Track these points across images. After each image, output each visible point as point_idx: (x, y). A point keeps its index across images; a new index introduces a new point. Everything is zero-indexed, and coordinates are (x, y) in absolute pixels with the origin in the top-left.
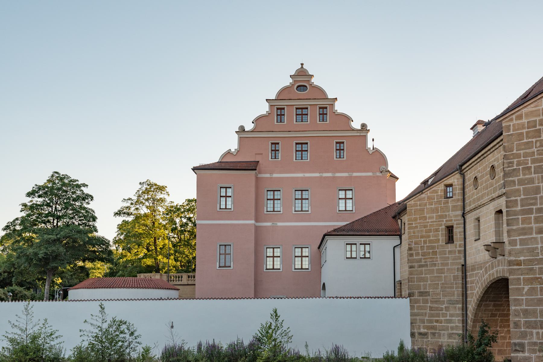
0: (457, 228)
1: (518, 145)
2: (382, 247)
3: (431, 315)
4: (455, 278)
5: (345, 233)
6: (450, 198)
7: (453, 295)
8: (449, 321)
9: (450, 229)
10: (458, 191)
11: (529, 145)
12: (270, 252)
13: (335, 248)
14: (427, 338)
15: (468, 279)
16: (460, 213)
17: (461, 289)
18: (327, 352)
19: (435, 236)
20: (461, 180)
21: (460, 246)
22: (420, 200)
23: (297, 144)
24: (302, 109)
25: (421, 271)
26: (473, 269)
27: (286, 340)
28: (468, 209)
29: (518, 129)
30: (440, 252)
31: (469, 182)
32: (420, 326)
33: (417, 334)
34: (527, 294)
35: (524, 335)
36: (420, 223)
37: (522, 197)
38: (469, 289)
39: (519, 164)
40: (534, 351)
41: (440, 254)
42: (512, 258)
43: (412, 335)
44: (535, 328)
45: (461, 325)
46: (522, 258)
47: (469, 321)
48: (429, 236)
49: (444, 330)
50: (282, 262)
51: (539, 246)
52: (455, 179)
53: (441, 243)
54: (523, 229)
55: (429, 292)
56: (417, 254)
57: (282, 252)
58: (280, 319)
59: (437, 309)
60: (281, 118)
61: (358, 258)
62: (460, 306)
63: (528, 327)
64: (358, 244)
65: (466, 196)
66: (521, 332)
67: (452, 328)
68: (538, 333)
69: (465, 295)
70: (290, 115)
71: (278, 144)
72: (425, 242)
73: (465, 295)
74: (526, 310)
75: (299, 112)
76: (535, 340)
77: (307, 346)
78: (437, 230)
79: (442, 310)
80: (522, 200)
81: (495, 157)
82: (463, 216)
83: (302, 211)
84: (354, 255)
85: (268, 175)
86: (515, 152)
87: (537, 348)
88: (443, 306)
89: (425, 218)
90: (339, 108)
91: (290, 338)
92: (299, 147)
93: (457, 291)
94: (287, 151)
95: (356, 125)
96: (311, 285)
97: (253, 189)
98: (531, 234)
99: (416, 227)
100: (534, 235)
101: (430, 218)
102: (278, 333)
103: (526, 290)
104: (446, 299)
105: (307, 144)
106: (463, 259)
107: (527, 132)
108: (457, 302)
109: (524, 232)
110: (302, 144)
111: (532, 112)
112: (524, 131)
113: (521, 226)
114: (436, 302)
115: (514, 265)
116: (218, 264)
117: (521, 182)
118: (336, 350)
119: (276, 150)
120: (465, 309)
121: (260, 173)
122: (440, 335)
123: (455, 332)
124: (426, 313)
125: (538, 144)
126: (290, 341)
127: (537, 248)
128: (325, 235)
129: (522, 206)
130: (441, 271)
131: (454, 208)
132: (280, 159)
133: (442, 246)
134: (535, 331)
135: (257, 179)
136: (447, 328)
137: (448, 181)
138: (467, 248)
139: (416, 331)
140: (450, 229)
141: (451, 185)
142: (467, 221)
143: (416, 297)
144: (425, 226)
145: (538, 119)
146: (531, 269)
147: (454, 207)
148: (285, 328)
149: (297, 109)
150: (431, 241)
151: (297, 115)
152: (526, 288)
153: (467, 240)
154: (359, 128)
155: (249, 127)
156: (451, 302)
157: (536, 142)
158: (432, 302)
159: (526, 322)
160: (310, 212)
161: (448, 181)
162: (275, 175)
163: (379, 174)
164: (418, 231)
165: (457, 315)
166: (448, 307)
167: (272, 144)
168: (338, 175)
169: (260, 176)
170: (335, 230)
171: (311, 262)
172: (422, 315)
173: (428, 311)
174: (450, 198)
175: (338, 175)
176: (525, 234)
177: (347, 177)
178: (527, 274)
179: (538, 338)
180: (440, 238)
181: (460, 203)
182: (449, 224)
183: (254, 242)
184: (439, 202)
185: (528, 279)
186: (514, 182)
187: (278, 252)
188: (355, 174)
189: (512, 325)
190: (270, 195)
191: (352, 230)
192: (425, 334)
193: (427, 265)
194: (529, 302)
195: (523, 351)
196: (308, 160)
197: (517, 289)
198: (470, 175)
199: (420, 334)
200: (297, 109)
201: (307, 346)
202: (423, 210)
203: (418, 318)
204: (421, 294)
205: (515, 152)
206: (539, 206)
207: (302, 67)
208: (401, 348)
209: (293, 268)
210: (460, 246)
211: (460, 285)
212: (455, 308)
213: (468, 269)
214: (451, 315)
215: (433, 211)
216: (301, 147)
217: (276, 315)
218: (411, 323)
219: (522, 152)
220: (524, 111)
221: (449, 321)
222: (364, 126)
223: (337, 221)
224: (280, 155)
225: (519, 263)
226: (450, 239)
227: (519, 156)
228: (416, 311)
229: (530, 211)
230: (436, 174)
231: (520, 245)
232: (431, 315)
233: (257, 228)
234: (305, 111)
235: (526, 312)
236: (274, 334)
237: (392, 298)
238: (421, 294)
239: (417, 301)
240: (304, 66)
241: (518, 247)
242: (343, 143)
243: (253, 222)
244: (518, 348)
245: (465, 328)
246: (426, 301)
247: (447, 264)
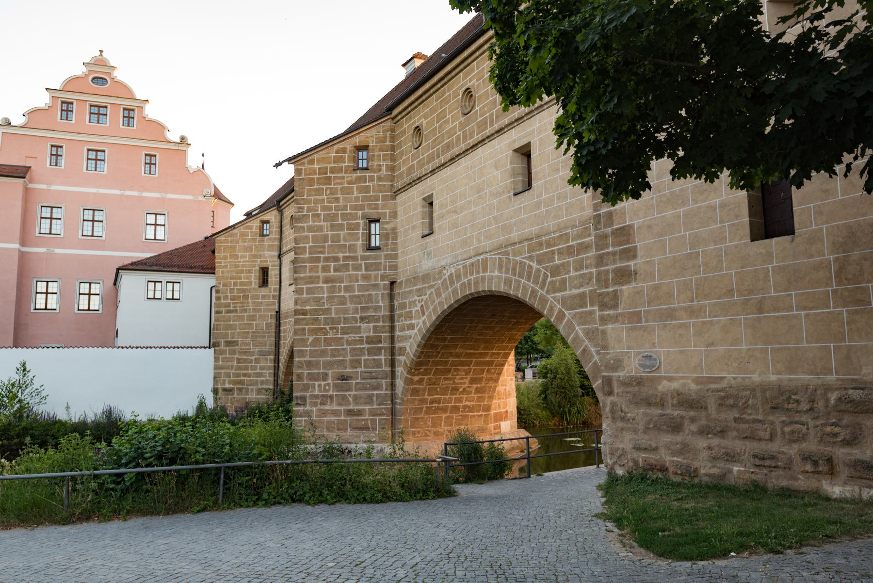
0: (272, 270)
1: (309, 191)
2: (196, 288)
3: (239, 368)
4: (268, 326)
5: (146, 267)
6: (266, 235)
7: (265, 345)
8: (259, 375)
9: (264, 271)
10: (275, 229)
11: (319, 191)
12: (41, 287)
13: (133, 285)
14: (233, 394)
15: (282, 328)
16: (276, 253)
17: (273, 339)
18: (96, 415)
19: (247, 278)
20: (279, 217)
21: (275, 291)
22: (231, 236)
23: (89, 150)
24: (99, 107)
25: (230, 317)
26: (286, 317)
27: (37, 401)
28: (284, 249)
29: (310, 174)
30: (252, 296)
31: (286, 221)
32: (224, 381)
33: (220, 391)
34: (311, 345)
35: (306, 388)
36: (230, 262)
37: (311, 244)
38: (282, 338)
39: (309, 210)
40: (315, 404)
41: (252, 299)
42: (299, 307)
43: (215, 391)
44: (318, 380)
45: (272, 379)
46: (308, 308)
47: (280, 374)
48: (240, 278)
49: (252, 385)
50: (61, 301)
51: (325, 296)
52: (272, 216)
53: (253, 286)
54: (310, 277)
55: (237, 342)
56: (226, 298)
57: (61, 288)
58: (30, 375)
59: (246, 361)
60: (67, 115)
61: (164, 298)
62: (272, 357)
63: (310, 380)
64: (164, 283)
65: (283, 236)
66: (304, 385)
67: (262, 383)
68: (320, 386)
69: (277, 345)
70: (80, 115)
71: (61, 147)
72: (235, 284)
73: (277, 345)
74: (310, 361)
75: (95, 110)
76: (317, 393)
77: (68, 408)
78: (250, 271)
79: (251, 362)
80: (310, 247)
81: (399, 185)
82: (280, 256)
83: (92, 236)
84: (158, 296)
85: (44, 187)
86: (305, 197)
87: (319, 401)
88: (253, 358)
89: (237, 256)
90: (150, 112)
91: (45, 398)
92: (92, 155)
93: (270, 340)
94: (74, 158)
95: (173, 136)
96: (100, 331)
97: (19, 204)
98: (318, 283)
99: (226, 266)
100: (321, 285)
101: (242, 257)
102: (26, 392)
103: (310, 341)
104: (257, 350)
105: (104, 151)
106: (277, 305)
107: (318, 178)
108: (269, 353)
109: (312, 280)
110: (97, 151)
111: (323, 158)
112: (316, 177)
113: (308, 274)
114: (245, 353)
115: (300, 314)
116: (76, 306)
117: (311, 229)
118: (109, 413)
119: (57, 155)
120: (277, 360)
121: (31, 182)
122: (247, 390)
123: (265, 386)
124: (232, 366)
125: (328, 192)
126: (43, 402)
127: (323, 298)
128: (118, 270)
129: (310, 254)
130: (252, 318)
131: (270, 248)
132: (63, 167)
133: (254, 289)
134: (317, 383)
135: (26, 190)
136: (256, 383)
137: (265, 217)
138: (282, 292)
139: (219, 386)
140: (264, 271)
141: (267, 222)
142: (283, 263)
143: (222, 347)
144: (236, 266)
145: (329, 166)
146: (317, 319)
147: (270, 246)
148: (35, 386)
149: (91, 106)
150: (242, 284)
151: (91, 113)
152: (311, 338)
153: (283, 284)
154: (179, 141)
155: (18, 120)
156: (262, 353)
157: (327, 189)
158: (240, 353)
159: (309, 374)
160: (104, 238)
161: (265, 217)
162: (54, 187)
163: (201, 198)
164: (228, 271)
165: (269, 368)
166: (259, 359)
167: (52, 146)
168: (145, 194)
169: (30, 186)
170: (132, 264)
171: (103, 302)
172: (228, 367)
173: (235, 364)
174: (266, 235)
175: (145, 194)
176: (312, 283)
177: (158, 198)
178: (313, 324)
179: (320, 391)
180: (253, 280)
181: (277, 243)
182: (264, 265)
183: (16, 272)
184: (254, 240)
185: (313, 330)
186: (303, 228)
187: (53, 287)
188: (170, 196)
189: (294, 377)
190: (46, 213)
191: (156, 265)
192: (230, 391)
193: (236, 311)
194: (312, 354)
195: (304, 405)
196: (105, 172)
197: (301, 339)
198: (289, 212)
199: (225, 390)
200: (91, 106)
201: (68, 408)
202: (234, 248)
203: (223, 371)
204: (228, 343)
205: (305, 197)
206: (326, 255)
207: (101, 55)
208: (201, 406)
209: (76, 308)
210: (275, 291)
211: (273, 334)
212: (267, 359)
213: (282, 316)
214: (262, 368)
215: (246, 249)
216: (96, 155)
217: (24, 369)
218: (215, 378)
219: (312, 198)
220: (316, 156)
221: (259, 375)
222: (183, 138)
223: (143, 252)
224: (63, 162)
225: (304, 313)
226: (264, 282)
227: (309, 202)
228: (221, 363)
229: (317, 260)
230: (261, 206)
231: (307, 294)
232: (239, 368)
233: (22, 256)
234: (102, 111)
235: (309, 364)
236: (19, 394)
237: (205, 348)
238: (228, 343)
239: (222, 352)
240: (103, 54)
241: (305, 296)
242: (155, 156)
243: (17, 246)
244: (299, 402)
245: (276, 382)
246: (234, 352)
247: (259, 310)
